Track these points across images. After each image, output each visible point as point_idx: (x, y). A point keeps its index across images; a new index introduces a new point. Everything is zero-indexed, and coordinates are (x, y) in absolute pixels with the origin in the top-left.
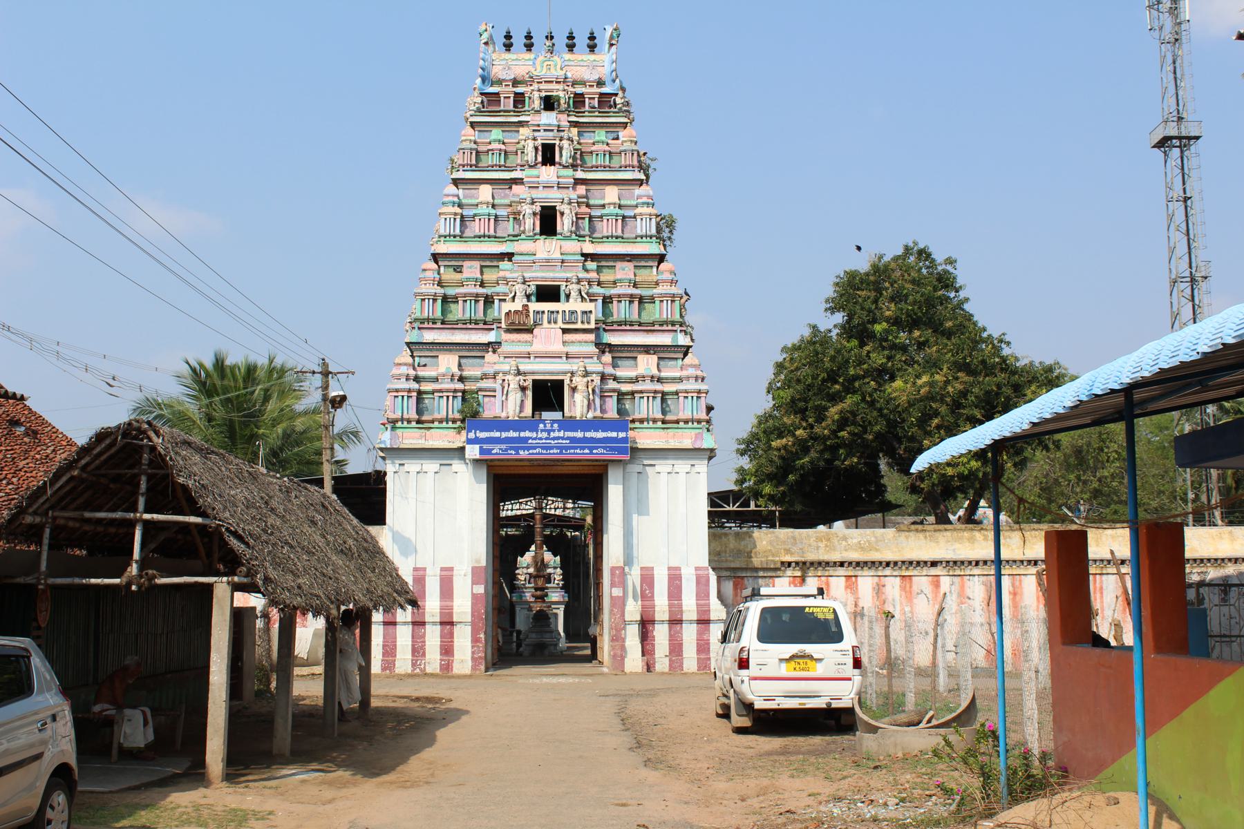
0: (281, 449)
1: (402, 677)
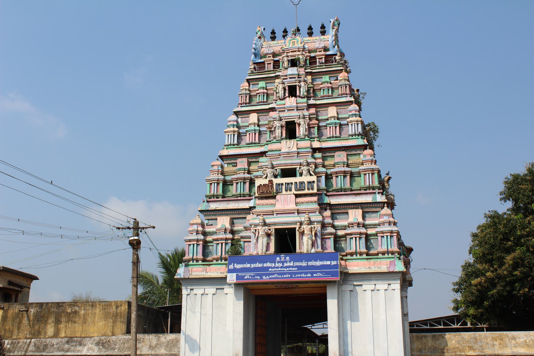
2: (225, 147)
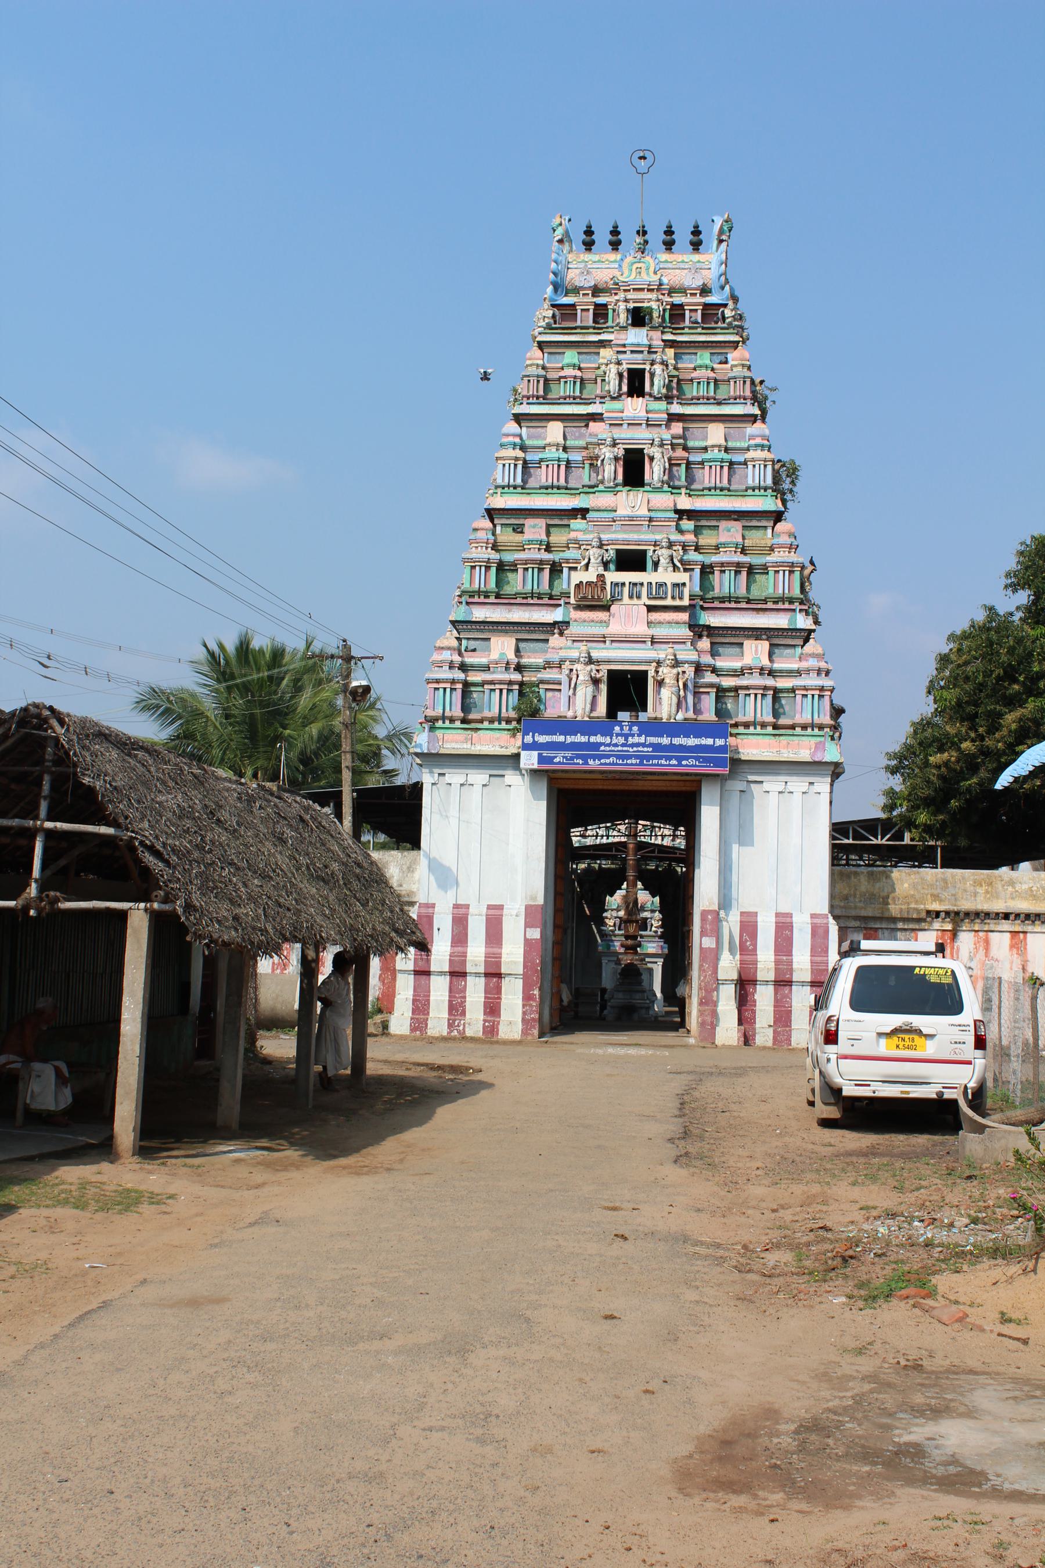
0: (316, 754)
1: (433, 1041)
2: (499, 490)
